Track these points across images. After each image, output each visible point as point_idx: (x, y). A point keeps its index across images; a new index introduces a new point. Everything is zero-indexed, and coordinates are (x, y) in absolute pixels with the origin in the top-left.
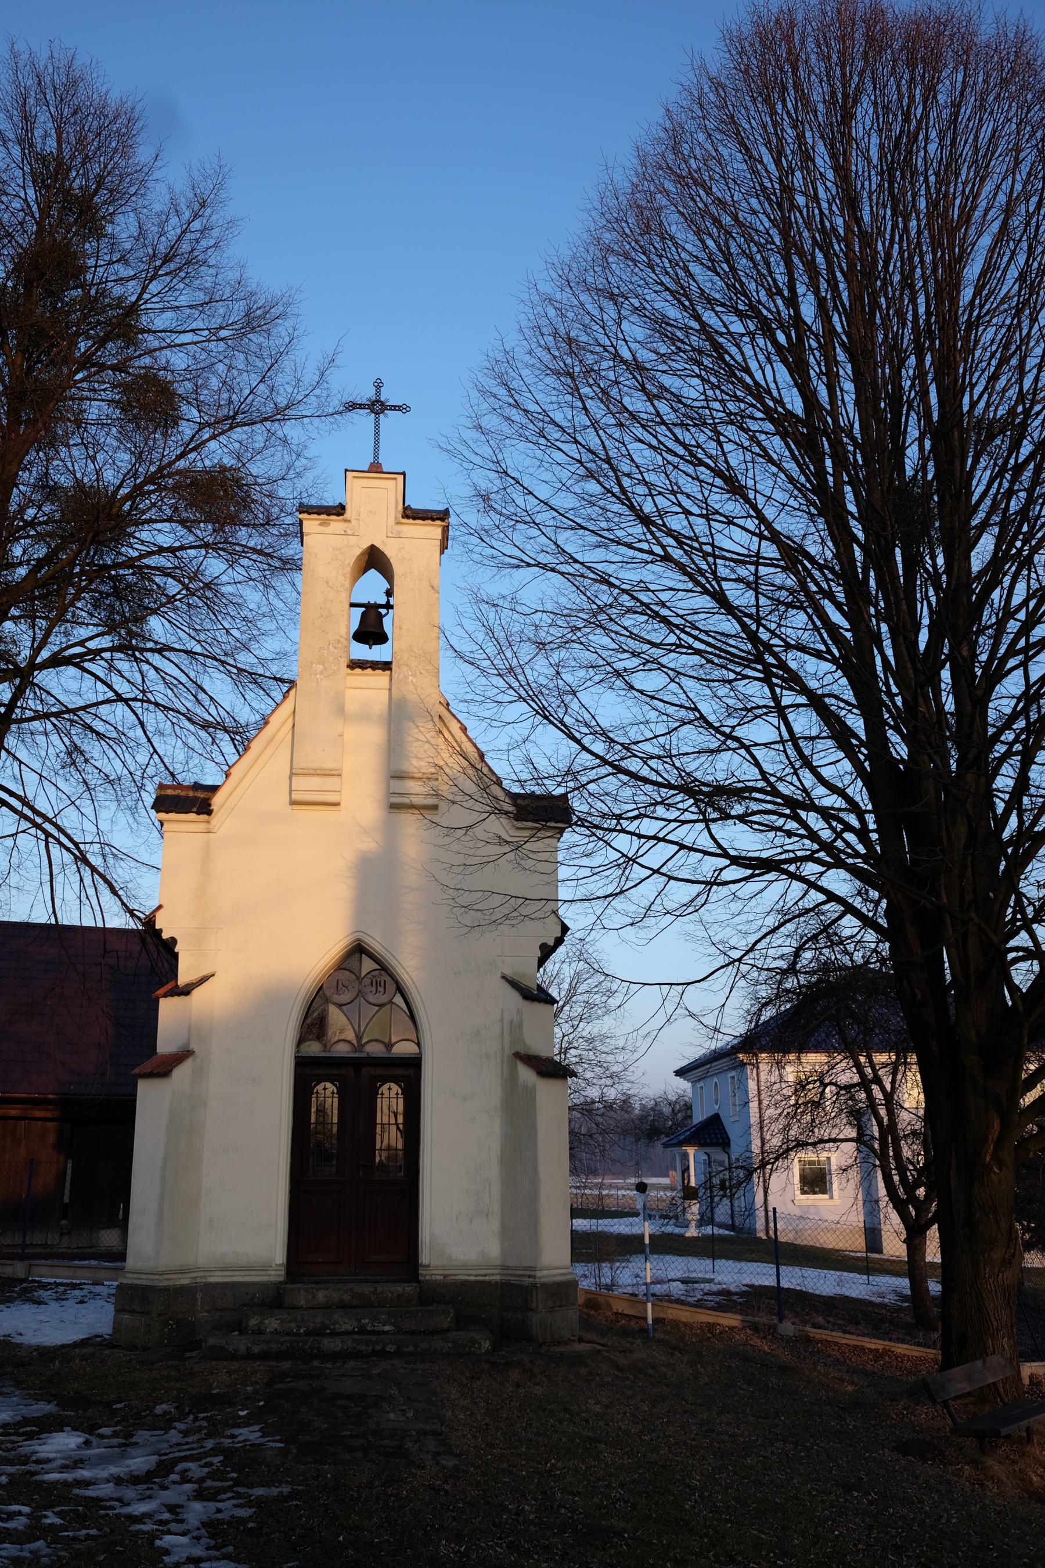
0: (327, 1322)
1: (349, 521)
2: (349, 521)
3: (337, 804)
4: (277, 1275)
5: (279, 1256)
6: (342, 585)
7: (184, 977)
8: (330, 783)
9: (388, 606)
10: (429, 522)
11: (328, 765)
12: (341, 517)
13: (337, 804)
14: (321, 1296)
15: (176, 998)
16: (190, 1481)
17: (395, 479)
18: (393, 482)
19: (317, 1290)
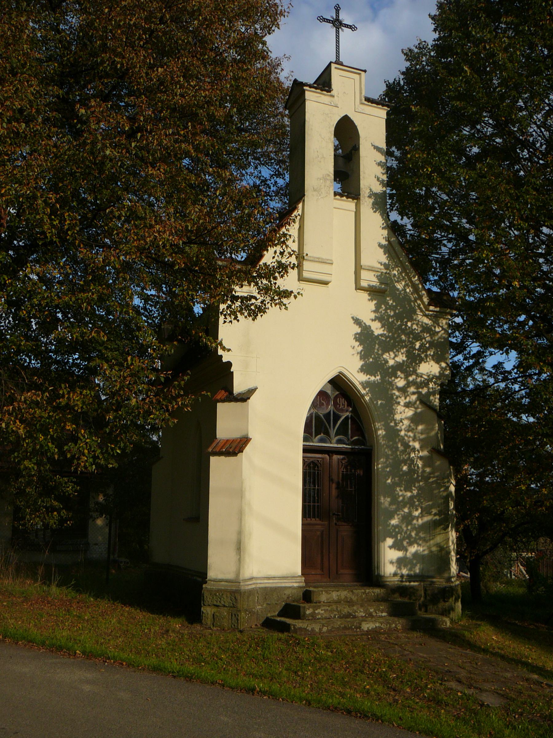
0: (351, 611)
1: (333, 96)
2: (333, 96)
3: (326, 283)
4: (298, 583)
5: (297, 569)
6: (330, 139)
7: (238, 387)
8: (325, 268)
9: (295, 297)
10: (380, 106)
11: (324, 256)
12: (329, 94)
13: (326, 283)
14: (335, 595)
15: (232, 404)
16: (60, 448)
17: (359, 74)
18: (358, 76)
19: (333, 591)
